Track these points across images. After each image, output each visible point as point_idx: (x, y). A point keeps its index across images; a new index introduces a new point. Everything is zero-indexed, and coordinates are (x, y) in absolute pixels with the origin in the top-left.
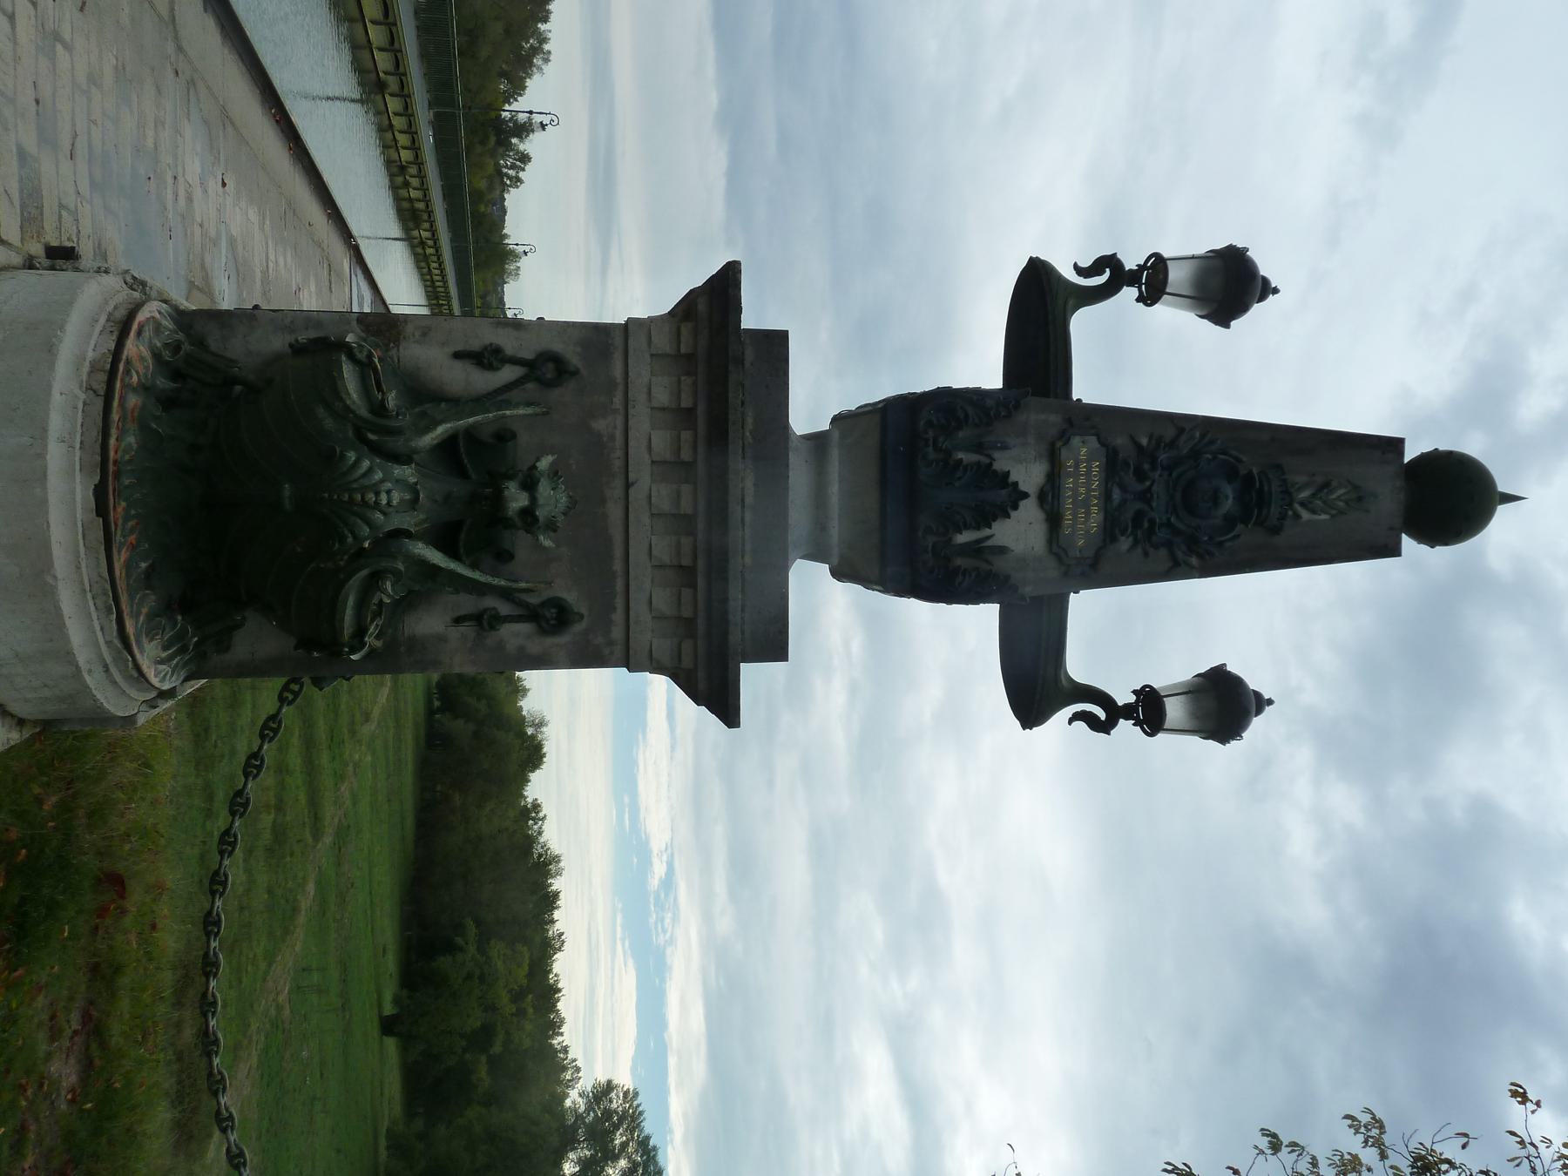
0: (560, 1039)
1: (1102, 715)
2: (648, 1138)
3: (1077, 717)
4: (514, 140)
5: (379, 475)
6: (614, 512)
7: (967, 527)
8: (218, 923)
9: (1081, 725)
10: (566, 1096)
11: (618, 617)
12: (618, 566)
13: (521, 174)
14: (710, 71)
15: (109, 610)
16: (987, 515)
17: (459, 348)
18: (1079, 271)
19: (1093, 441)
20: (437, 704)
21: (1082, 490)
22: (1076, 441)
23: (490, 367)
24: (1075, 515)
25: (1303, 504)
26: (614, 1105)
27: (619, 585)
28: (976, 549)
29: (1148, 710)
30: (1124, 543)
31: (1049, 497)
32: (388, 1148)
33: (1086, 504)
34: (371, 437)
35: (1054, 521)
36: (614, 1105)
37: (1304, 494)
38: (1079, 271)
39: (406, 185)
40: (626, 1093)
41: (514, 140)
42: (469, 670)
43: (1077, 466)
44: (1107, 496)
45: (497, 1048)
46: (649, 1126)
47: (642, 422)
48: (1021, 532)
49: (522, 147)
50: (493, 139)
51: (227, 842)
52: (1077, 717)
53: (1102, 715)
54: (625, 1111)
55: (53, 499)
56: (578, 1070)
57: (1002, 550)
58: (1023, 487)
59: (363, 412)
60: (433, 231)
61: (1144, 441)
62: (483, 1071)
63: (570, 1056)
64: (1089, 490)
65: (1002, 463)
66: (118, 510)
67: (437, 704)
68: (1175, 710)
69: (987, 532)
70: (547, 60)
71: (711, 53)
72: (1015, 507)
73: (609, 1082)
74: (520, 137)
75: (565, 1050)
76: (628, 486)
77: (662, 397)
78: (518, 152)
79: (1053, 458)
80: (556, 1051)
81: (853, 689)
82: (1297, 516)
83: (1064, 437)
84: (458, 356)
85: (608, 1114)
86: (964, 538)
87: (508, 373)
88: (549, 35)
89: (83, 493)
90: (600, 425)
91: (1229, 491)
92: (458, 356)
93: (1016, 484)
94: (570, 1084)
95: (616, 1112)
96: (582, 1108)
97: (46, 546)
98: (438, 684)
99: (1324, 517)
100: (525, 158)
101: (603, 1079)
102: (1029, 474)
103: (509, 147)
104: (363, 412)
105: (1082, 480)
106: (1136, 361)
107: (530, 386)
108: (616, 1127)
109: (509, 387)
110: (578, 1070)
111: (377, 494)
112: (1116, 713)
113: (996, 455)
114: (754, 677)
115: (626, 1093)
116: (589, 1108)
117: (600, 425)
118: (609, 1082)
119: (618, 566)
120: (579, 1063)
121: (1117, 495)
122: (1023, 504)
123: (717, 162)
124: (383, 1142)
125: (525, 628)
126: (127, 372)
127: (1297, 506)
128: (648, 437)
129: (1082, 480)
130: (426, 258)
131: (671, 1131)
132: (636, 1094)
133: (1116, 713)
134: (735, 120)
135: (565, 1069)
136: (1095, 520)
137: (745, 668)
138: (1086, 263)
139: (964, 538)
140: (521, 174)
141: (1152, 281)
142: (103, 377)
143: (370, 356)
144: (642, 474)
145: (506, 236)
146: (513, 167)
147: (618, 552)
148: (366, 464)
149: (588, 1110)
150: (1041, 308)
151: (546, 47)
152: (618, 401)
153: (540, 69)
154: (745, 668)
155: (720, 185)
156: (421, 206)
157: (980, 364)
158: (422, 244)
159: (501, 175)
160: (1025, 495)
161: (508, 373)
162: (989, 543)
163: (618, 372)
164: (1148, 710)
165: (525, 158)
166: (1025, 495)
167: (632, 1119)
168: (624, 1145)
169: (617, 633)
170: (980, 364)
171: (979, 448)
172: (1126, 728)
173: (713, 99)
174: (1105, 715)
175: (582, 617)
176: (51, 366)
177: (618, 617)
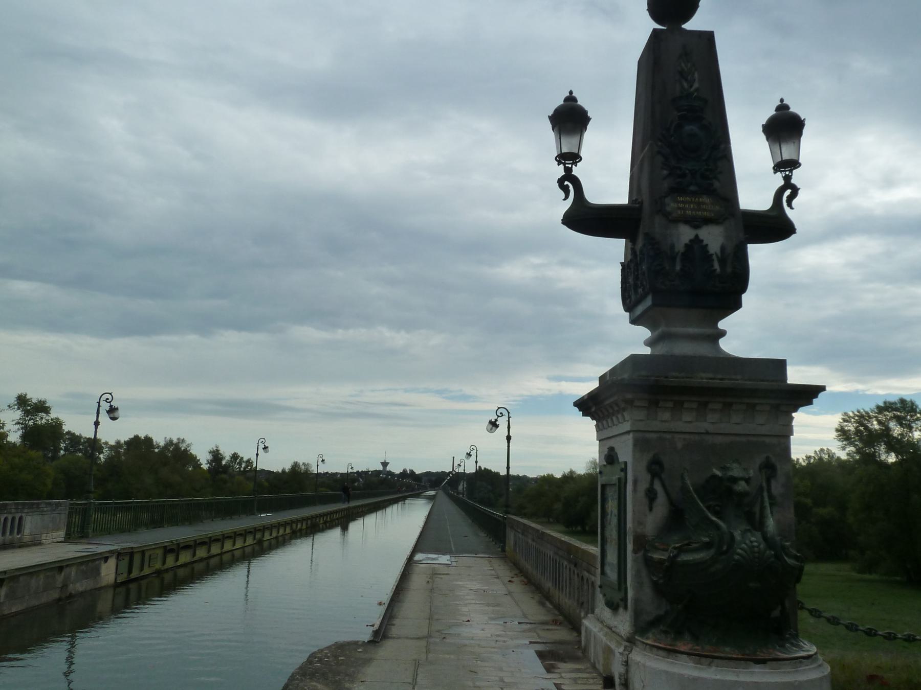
0: (801, 461)
1: (788, 192)
2: (878, 407)
3: (790, 205)
4: (224, 463)
5: (744, 546)
6: (719, 440)
7: (712, 266)
8: (890, 634)
9: (795, 202)
10: (839, 458)
11: (767, 440)
12: (744, 439)
13: (245, 459)
14: (174, 338)
15: (801, 662)
16: (707, 257)
17: (647, 508)
18: (567, 197)
19: (667, 200)
20: (579, 528)
21: (692, 206)
22: (668, 209)
23: (656, 494)
24: (705, 210)
25: (691, 86)
26: (852, 429)
27: (754, 439)
28: (722, 261)
29: (786, 166)
30: (717, 184)
31: (696, 223)
32: (870, 573)
33: (699, 204)
34: (725, 548)
35: (708, 221)
36: (852, 429)
37: (685, 85)
38: (567, 197)
39: (301, 530)
40: (845, 420)
41: (224, 463)
42: (792, 510)
43: (680, 208)
44: (694, 194)
45: (809, 501)
46: (868, 406)
47: (679, 426)
48: (714, 238)
49: (228, 458)
50: (224, 476)
51: (852, 627)
52: (790, 205)
53: (788, 192)
54: (857, 422)
55: (764, 680)
56: (822, 450)
57: (723, 248)
58: (692, 237)
59: (712, 552)
60: (321, 516)
61: (665, 172)
62: (823, 511)
63: (813, 455)
64: (691, 202)
65: (680, 247)
66: (761, 655)
67: (579, 528)
68: (787, 153)
69: (714, 257)
70: (183, 440)
71: (163, 338)
72: (702, 241)
73: (837, 430)
74: (223, 458)
75: (809, 458)
76: (707, 433)
77: (667, 416)
78: (231, 461)
79: (676, 221)
80: (809, 463)
81: (564, 263)
82: (697, 90)
83: (666, 215)
84: (651, 509)
85: (857, 431)
86: (716, 266)
87: (658, 486)
88: (168, 438)
89: (757, 669)
90: (679, 445)
91: (689, 128)
92: (651, 509)
93: (691, 241)
94: (831, 455)
95: (856, 428)
96: (852, 449)
97: (784, 684)
98: (567, 526)
99: (696, 75)
100: (235, 457)
101: (835, 434)
102: (685, 234)
103: (226, 467)
104: (712, 552)
105: (687, 206)
106: (609, 168)
107: (663, 476)
108: (866, 428)
109: (664, 486)
110: (822, 450)
111: (754, 547)
112: (788, 184)
113: (676, 250)
114: (795, 376)
115: (845, 420)
116: (851, 443)
117: (679, 445)
118: (837, 430)
119: (744, 439)
120: (818, 449)
121: (693, 188)
122: (701, 237)
123: (231, 337)
124: (867, 576)
125: (773, 484)
126: (696, 650)
127: (692, 90)
128: (687, 422)
129: (687, 206)
130: (332, 521)
131: (857, 391)
132: (846, 414)
133: (788, 184)
134: (206, 324)
135: (821, 459)
136: (705, 199)
137: (790, 381)
138: (563, 195)
139: (716, 266)
140: (245, 459)
141: (569, 158)
142: (703, 660)
143: (675, 548)
144: (703, 426)
145: (283, 471)
146: (240, 464)
147: (738, 439)
148: (739, 551)
149: (855, 446)
150: (586, 218)
151: (175, 441)
152: (668, 436)
153: (188, 446)
154: (790, 381)
155: (245, 336)
156: (309, 522)
157: (614, 249)
158: (325, 522)
159: (245, 472)
160: (697, 236)
161: (658, 486)
162: (719, 254)
163: (654, 436)
164: (786, 166)
165: (235, 457)
166: (697, 236)
167: (862, 418)
168: (880, 422)
169: (775, 441)
170: (614, 249)
171: (673, 258)
172: (797, 177)
173: (192, 338)
174: (790, 189)
175: (768, 458)
176: (703, 679)
177: (767, 440)
